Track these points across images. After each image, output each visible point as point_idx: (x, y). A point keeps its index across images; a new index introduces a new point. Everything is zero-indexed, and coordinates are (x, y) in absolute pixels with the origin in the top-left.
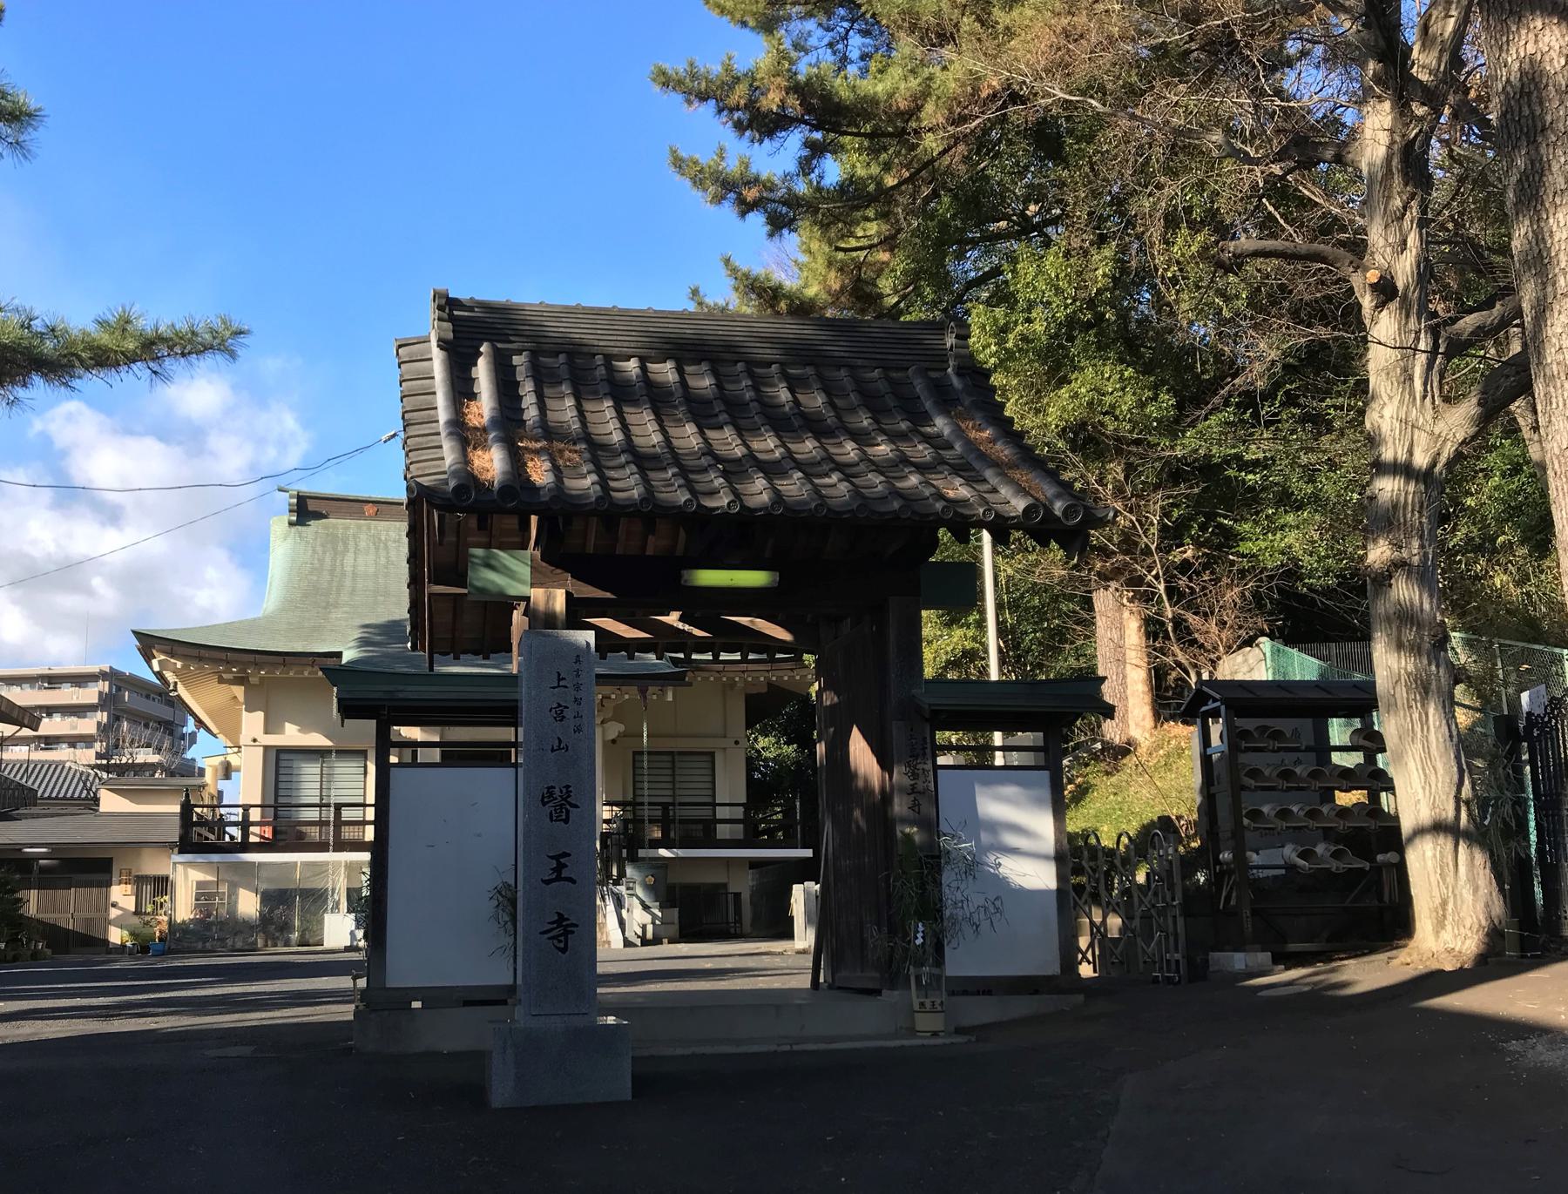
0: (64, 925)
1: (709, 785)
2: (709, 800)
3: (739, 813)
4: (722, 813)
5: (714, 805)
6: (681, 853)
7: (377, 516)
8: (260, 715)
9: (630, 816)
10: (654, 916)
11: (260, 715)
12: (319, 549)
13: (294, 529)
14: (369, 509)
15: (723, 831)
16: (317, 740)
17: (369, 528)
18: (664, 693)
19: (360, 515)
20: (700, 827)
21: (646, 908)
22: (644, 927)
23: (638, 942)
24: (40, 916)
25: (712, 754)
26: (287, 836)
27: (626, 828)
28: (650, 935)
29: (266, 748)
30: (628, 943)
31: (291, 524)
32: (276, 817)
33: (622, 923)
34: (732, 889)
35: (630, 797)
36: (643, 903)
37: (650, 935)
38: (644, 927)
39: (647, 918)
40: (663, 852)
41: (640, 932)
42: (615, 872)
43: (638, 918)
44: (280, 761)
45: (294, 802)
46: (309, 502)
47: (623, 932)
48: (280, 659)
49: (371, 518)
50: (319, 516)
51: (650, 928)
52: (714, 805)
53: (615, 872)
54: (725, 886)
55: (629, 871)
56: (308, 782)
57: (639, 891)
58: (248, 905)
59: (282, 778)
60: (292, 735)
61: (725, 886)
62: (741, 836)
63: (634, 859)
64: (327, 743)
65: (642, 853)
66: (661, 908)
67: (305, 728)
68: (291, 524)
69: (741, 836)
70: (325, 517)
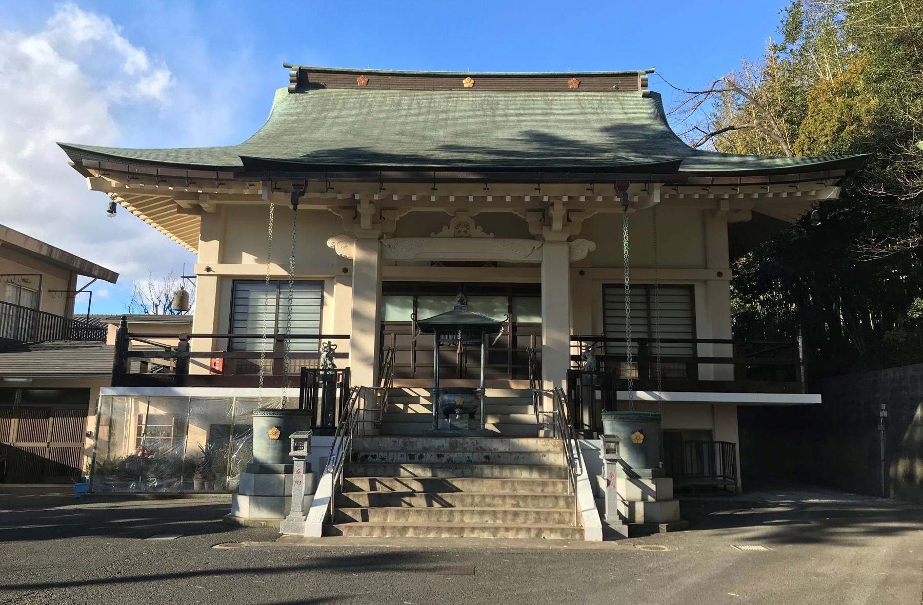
0: (40, 454)
1: (688, 322)
2: (688, 337)
3: (728, 351)
4: (704, 350)
5: (695, 341)
6: (664, 396)
7: (368, 86)
8: (215, 244)
9: (600, 352)
10: (645, 490)
11: (215, 244)
12: (309, 108)
13: (292, 95)
14: (362, 80)
15: (706, 372)
16: (274, 270)
17: (359, 95)
18: (649, 192)
19: (353, 85)
20: (682, 366)
21: (633, 477)
22: (631, 506)
23: (624, 530)
24: (19, 444)
25: (690, 289)
26: (237, 368)
27: (598, 366)
28: (640, 517)
29: (221, 278)
30: (609, 533)
31: (291, 91)
32: (230, 349)
33: (599, 497)
34: (719, 437)
35: (600, 332)
36: (627, 469)
37: (640, 517)
38: (631, 506)
39: (635, 493)
40: (642, 395)
41: (624, 511)
42: (586, 419)
43: (623, 490)
44: (235, 293)
45: (250, 332)
46: (310, 75)
47: (602, 516)
48: (213, 175)
49: (362, 88)
50: (317, 86)
51: (640, 507)
52: (695, 341)
53: (586, 419)
54: (709, 433)
55: (609, 426)
56: (265, 313)
57: (624, 453)
58: (196, 439)
59: (238, 309)
60: (248, 265)
61: (709, 433)
62: (731, 378)
63: (611, 405)
64: (282, 272)
65: (621, 395)
66: (655, 477)
67: (264, 257)
68: (291, 91)
69: (731, 378)
70: (323, 87)
